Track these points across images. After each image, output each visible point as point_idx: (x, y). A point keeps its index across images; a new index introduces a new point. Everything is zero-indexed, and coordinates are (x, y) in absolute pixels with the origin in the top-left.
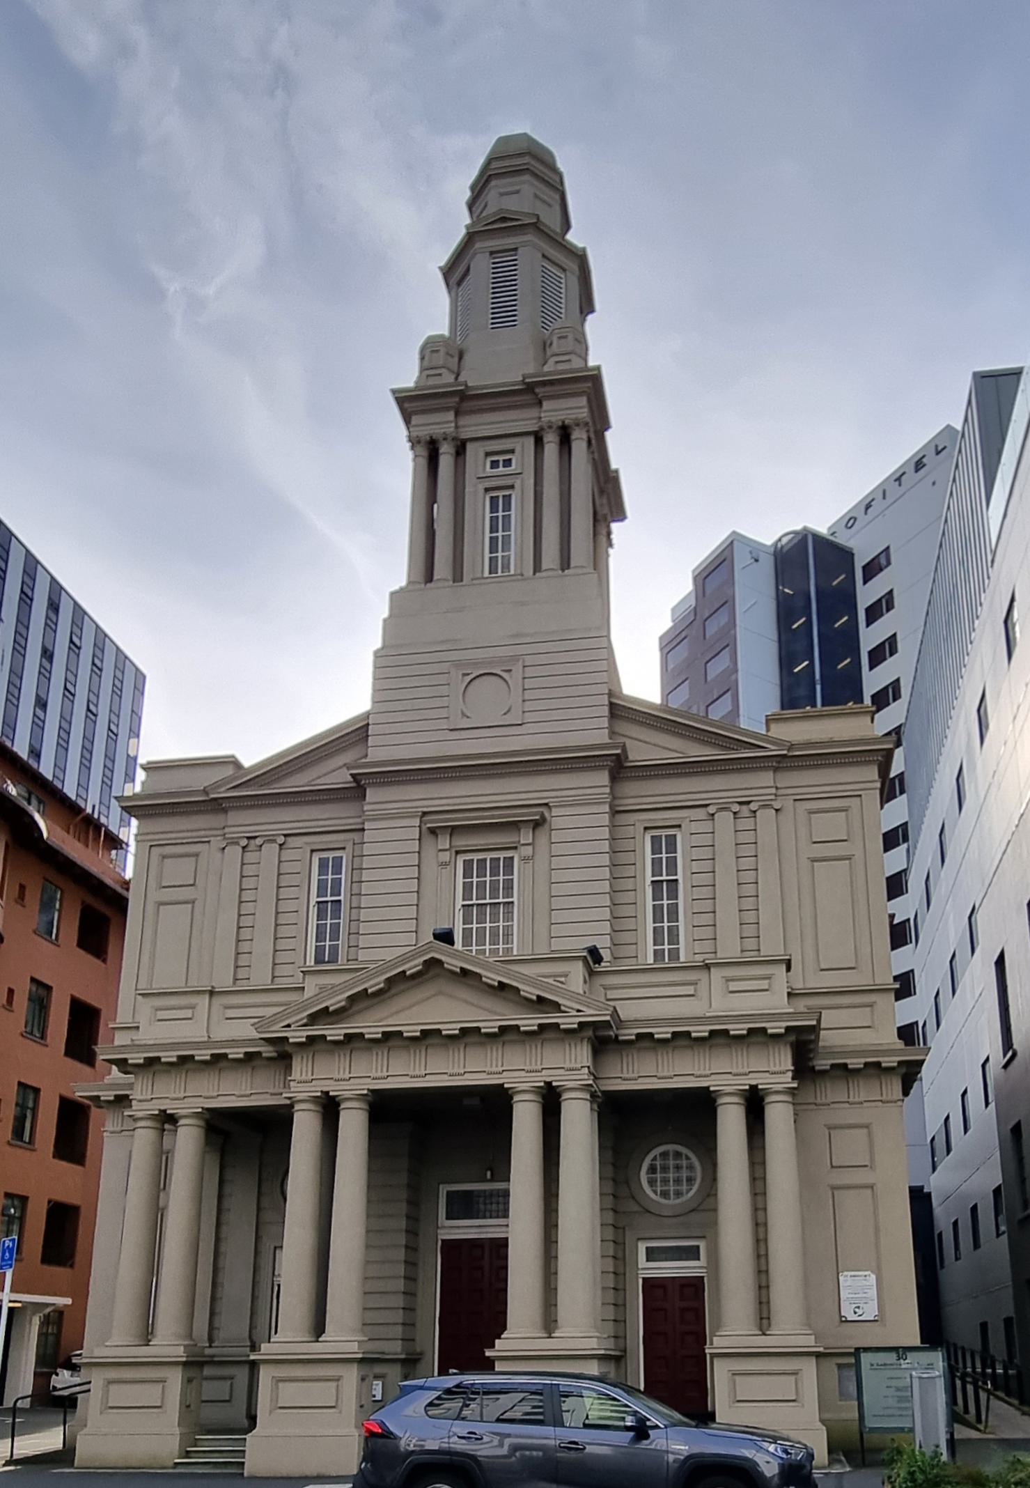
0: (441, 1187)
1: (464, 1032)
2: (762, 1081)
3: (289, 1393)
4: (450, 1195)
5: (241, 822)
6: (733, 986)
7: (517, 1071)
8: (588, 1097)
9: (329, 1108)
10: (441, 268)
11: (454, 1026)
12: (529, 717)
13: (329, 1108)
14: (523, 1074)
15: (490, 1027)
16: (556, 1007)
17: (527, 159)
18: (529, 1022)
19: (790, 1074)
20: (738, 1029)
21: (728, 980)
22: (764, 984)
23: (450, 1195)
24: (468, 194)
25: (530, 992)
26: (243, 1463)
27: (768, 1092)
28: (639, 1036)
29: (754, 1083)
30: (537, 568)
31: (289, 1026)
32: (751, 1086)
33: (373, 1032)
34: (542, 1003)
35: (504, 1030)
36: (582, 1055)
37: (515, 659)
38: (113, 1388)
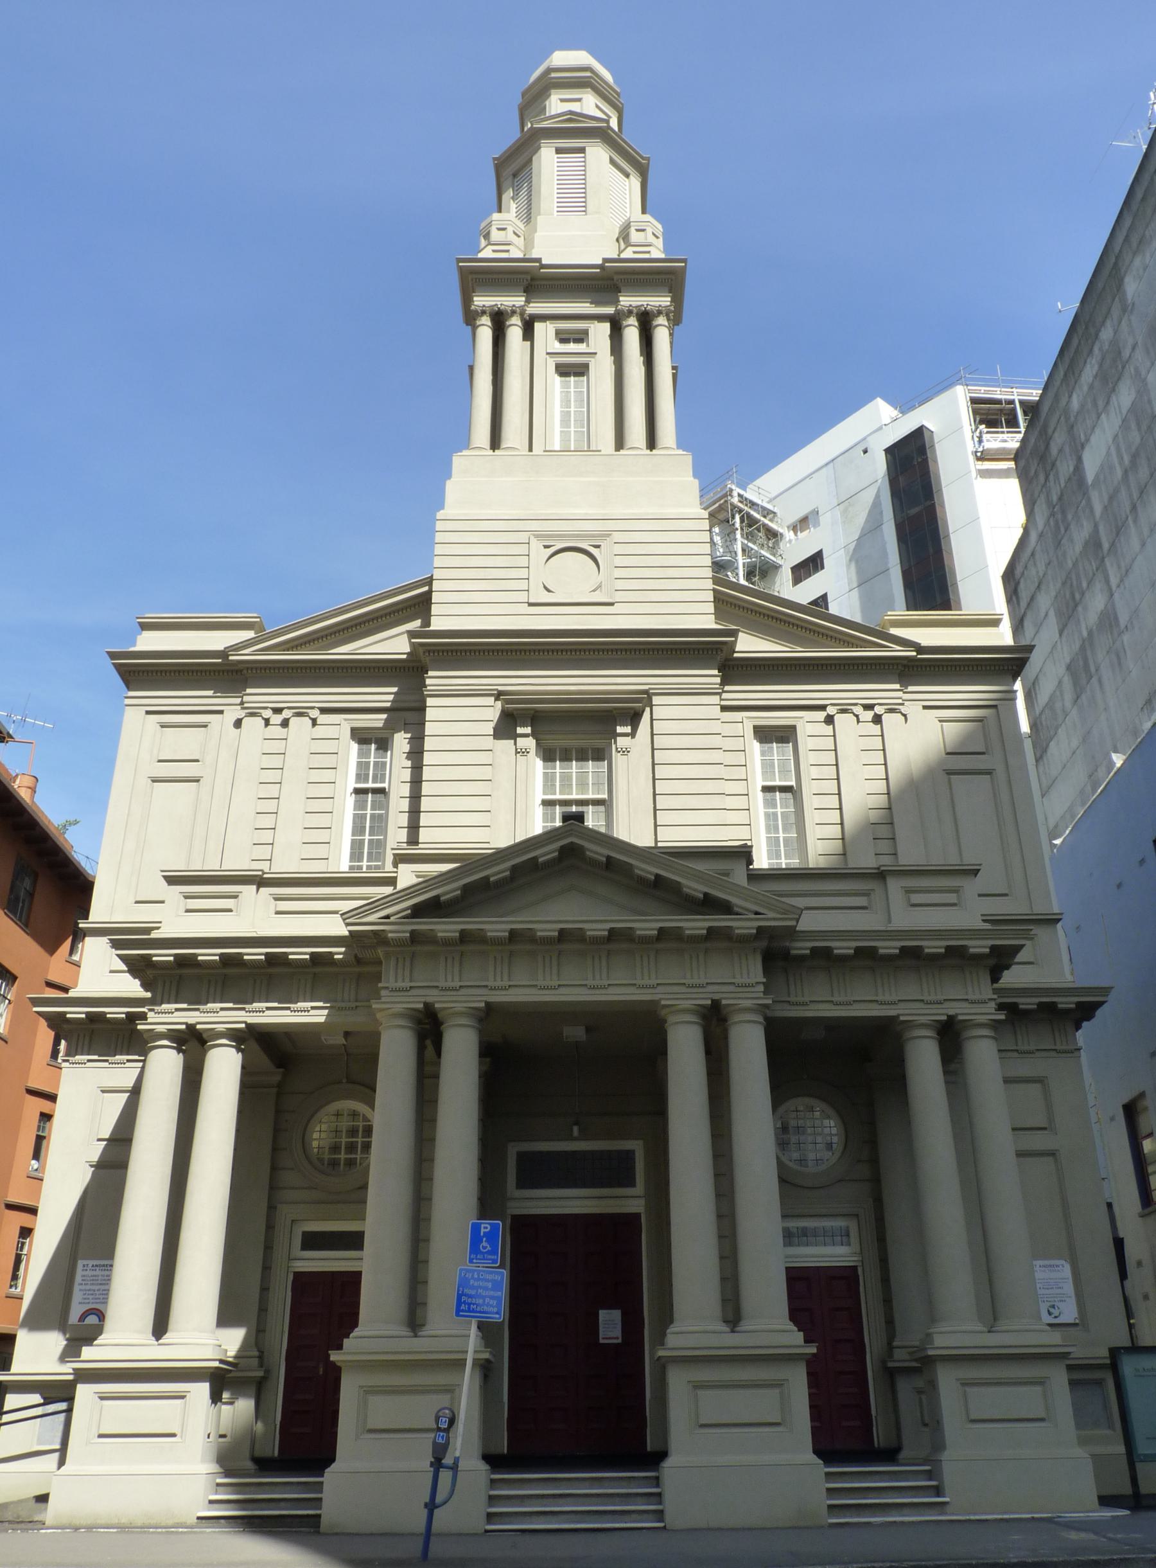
1: (563, 935)
2: (961, 1011)
3: (714, 1405)
4: (522, 1157)
5: (259, 696)
6: (917, 898)
7: (674, 990)
8: (761, 1019)
9: (429, 1029)
10: (494, 159)
11: (600, 926)
12: (618, 597)
13: (429, 1029)
14: (683, 989)
16: (725, 908)
17: (588, 74)
18: (647, 926)
19: (761, 988)
20: (934, 947)
21: (909, 891)
22: (951, 898)
23: (522, 1157)
24: (519, 100)
25: (695, 888)
27: (968, 1024)
28: (814, 950)
29: (951, 1012)
30: (620, 443)
31: (387, 917)
34: (710, 904)
35: (614, 935)
36: (753, 971)
37: (606, 535)
38: (374, 1400)
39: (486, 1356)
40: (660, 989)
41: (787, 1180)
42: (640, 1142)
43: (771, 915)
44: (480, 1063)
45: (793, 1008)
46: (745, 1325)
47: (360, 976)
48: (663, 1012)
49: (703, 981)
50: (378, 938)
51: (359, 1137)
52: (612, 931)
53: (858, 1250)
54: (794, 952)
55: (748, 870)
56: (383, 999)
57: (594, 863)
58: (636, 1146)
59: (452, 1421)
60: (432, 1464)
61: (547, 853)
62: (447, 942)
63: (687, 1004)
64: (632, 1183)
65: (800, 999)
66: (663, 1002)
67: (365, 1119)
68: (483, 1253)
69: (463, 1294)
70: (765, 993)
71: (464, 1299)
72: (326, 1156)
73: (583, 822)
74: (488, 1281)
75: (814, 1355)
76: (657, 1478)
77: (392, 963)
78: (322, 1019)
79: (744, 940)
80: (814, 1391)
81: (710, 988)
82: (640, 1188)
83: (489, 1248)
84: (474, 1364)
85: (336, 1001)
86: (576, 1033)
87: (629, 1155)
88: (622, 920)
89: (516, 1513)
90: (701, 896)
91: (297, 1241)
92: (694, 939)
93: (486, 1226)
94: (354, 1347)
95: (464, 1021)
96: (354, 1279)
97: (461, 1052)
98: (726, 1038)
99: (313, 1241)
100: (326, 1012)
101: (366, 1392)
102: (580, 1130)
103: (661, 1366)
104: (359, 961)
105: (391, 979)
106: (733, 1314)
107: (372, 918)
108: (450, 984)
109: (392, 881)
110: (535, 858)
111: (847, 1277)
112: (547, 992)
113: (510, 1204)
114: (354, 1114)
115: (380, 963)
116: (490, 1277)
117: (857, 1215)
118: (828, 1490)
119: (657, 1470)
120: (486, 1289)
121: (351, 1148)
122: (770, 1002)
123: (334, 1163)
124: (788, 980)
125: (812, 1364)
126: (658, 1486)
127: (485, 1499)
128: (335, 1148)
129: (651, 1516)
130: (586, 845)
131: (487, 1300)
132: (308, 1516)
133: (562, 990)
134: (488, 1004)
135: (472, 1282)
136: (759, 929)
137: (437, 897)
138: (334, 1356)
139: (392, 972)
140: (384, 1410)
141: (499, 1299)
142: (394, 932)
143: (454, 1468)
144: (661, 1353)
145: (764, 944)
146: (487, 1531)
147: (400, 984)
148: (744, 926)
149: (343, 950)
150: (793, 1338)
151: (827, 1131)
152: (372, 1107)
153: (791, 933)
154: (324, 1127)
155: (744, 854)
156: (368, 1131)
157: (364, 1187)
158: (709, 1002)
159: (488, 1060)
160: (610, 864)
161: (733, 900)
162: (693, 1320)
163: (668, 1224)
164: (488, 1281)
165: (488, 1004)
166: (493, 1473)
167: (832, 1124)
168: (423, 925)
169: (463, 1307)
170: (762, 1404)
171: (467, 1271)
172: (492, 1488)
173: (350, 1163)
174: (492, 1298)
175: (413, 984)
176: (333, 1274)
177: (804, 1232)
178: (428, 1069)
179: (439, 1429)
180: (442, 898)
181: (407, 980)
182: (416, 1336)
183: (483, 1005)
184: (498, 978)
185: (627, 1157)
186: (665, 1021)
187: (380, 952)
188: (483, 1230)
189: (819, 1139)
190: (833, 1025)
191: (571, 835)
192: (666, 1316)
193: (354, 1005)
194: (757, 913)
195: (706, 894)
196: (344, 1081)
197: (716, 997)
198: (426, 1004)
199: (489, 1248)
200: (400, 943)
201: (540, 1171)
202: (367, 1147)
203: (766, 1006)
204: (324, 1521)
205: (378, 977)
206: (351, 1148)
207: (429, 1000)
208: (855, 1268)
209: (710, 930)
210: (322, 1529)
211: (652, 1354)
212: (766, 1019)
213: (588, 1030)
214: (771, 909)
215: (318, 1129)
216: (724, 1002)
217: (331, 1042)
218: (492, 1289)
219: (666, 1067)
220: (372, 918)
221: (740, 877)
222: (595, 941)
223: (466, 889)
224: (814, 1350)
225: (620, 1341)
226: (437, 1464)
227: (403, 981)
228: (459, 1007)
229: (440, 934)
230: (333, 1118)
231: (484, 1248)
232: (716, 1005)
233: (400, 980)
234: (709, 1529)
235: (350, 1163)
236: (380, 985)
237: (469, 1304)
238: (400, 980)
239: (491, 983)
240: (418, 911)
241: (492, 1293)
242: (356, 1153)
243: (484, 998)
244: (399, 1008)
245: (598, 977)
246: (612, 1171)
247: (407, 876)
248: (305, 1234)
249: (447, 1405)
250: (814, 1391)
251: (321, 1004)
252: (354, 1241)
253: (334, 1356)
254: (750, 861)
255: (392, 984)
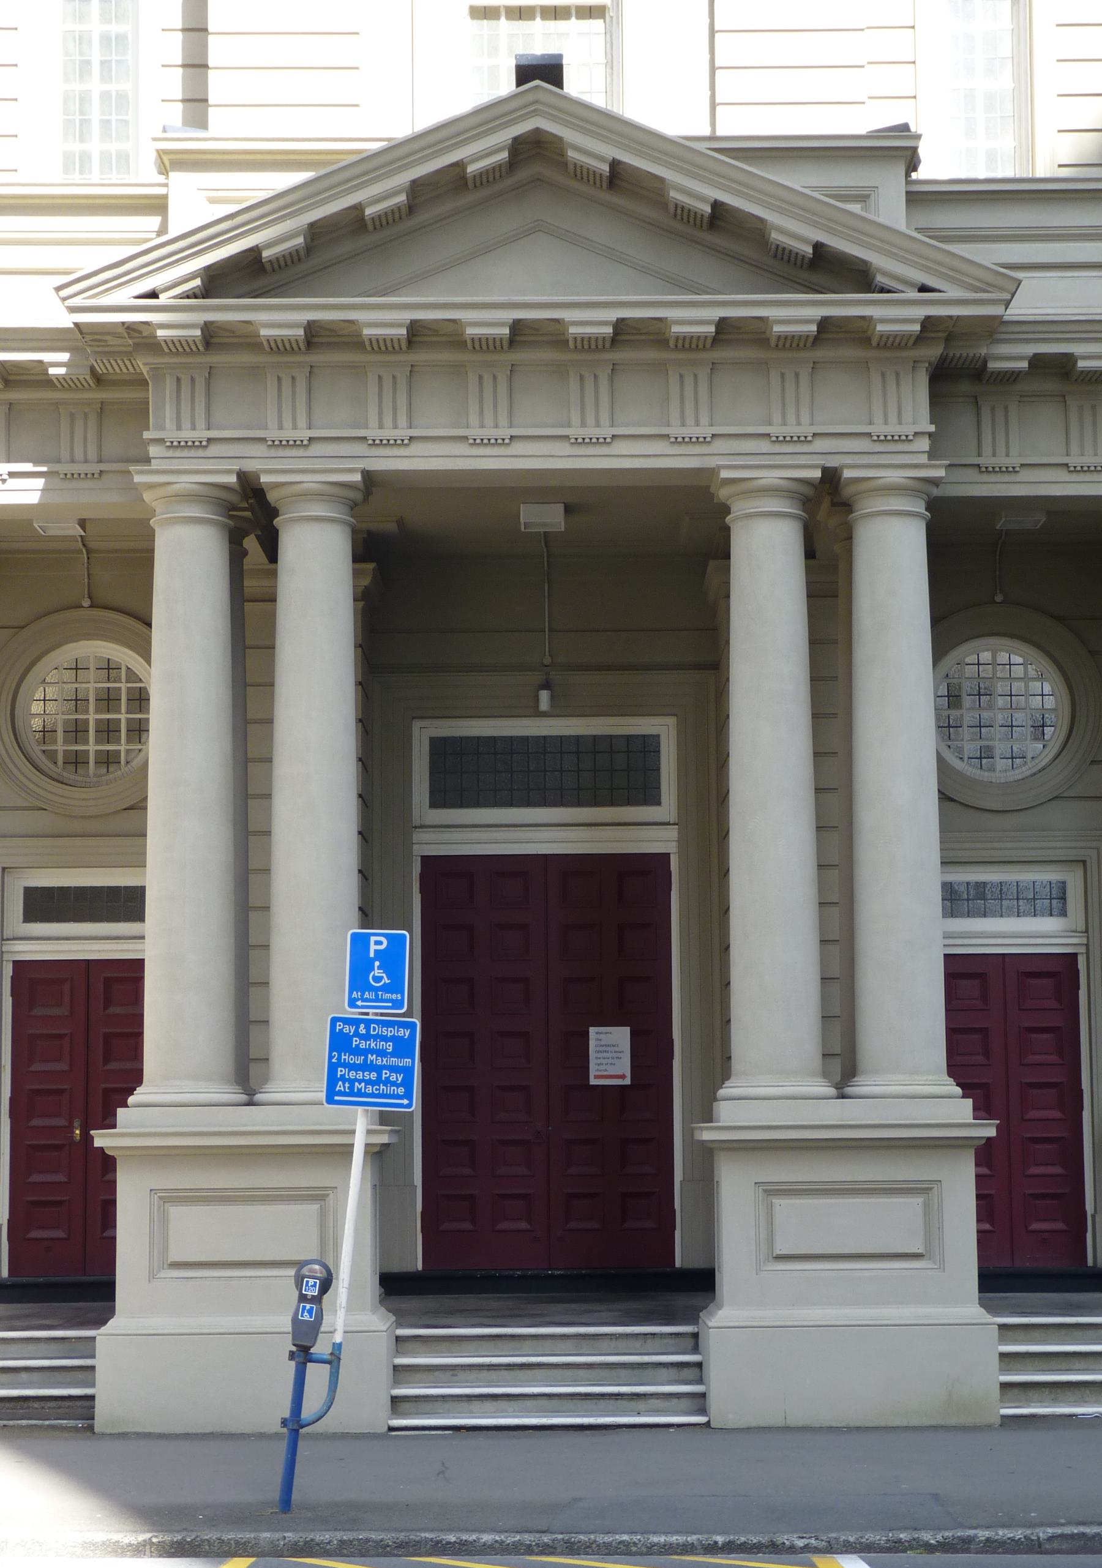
0: (417, 725)
1: (520, 333)
4: (440, 748)
7: (746, 446)
8: (920, 507)
9: (251, 521)
14: (764, 446)
15: (595, 322)
16: (858, 277)
18: (693, 315)
19: (924, 444)
23: (440, 748)
25: (797, 233)
26: (92, 1398)
28: (1037, 361)
31: (153, 295)
32: (825, 470)
33: (487, 322)
34: (826, 268)
35: (623, 333)
36: (910, 408)
39: (384, 1139)
40: (719, 446)
41: (958, 801)
42: (671, 721)
43: (953, 292)
44: (356, 574)
45: (986, 478)
46: (864, 1085)
47: (103, 409)
48: (723, 494)
49: (807, 430)
50: (139, 338)
51: (124, 710)
52: (620, 326)
53: (1081, 926)
54: (993, 365)
55: (909, 182)
56: (155, 465)
57: (582, 174)
58: (664, 730)
59: (326, 1284)
60: (292, 1356)
61: (484, 153)
62: (280, 348)
63: (771, 477)
64: (651, 797)
65: (1002, 460)
66: (724, 474)
67: (132, 676)
68: (372, 989)
69: (340, 1064)
70: (932, 454)
71: (341, 1071)
72: (60, 747)
73: (559, 84)
74: (385, 1039)
75: (989, 1139)
76: (695, 1336)
77: (169, 384)
78: (33, 498)
79: (893, 344)
80: (985, 1171)
81: (819, 445)
82: (668, 806)
83: (386, 980)
84: (366, 1153)
85: (59, 461)
86: (549, 518)
87: (648, 746)
88: (641, 303)
89: (444, 1397)
90: (809, 250)
91: (16, 905)
92: (791, 343)
93: (378, 941)
94: (132, 1127)
95: (319, 510)
96: (127, 977)
97: (317, 575)
98: (848, 538)
99: (45, 905)
100: (40, 483)
101: (164, 1200)
102: (553, 698)
103: (706, 1157)
104: (99, 380)
105: (168, 421)
106: (843, 1062)
107: (124, 296)
108: (289, 434)
109: (157, 206)
110: (460, 165)
111: (1057, 975)
112: (489, 451)
113: (418, 836)
114: (109, 668)
115: (143, 383)
116: (389, 1032)
117: (1084, 862)
118: (1002, 1355)
119: (694, 1319)
120: (382, 1053)
121: (108, 731)
122: (941, 473)
123: (77, 761)
124: (978, 414)
125: (985, 1153)
126: (696, 1350)
127: (386, 1374)
128: (77, 731)
129: (684, 1403)
130: (568, 135)
131: (385, 1074)
132: (70, 1398)
133: (518, 448)
134: (367, 475)
135: (355, 1041)
136: (928, 323)
137: (255, 251)
138: (101, 1139)
139: (169, 412)
140: (197, 1231)
141: (408, 1072)
142: (170, 323)
143: (334, 1360)
144: (707, 1136)
145: (934, 352)
146: (391, 1429)
147: (187, 434)
148: (894, 315)
149: (65, 357)
150: (955, 1112)
151: (1036, 702)
152: (147, 656)
153: (992, 329)
154: (51, 692)
155: (897, 149)
156: (140, 699)
157: (140, 806)
158: (817, 474)
159: (371, 566)
160: (617, 177)
161: (876, 259)
162: (766, 1076)
163: (725, 873)
164: (385, 1039)
165: (367, 475)
166: (400, 1325)
167: (1047, 688)
168: (228, 312)
169: (340, 1087)
170: (894, 1221)
171: (347, 1021)
172: (398, 1353)
173: (108, 760)
174: (394, 1069)
175: (213, 434)
176: (88, 965)
177: (980, 890)
178: (250, 584)
179: (303, 1298)
180: (265, 254)
181: (201, 423)
182: (250, 1103)
183: (357, 477)
184: (388, 421)
185: (646, 749)
186: (726, 510)
187: (143, 364)
188: (373, 948)
189: (1019, 717)
190: (1059, 510)
191: (534, 113)
192: (718, 1063)
193: (96, 468)
194: (923, 289)
195: (818, 247)
196: (86, 603)
197: (832, 462)
198: (242, 476)
199: (386, 980)
200: (178, 347)
201: (471, 774)
202: (139, 730)
203: (935, 482)
204: (101, 1408)
205: (140, 414)
206: (108, 731)
207: (250, 466)
208: (1074, 956)
209: (824, 324)
210: (99, 1424)
211: (688, 1133)
212: (935, 505)
213: (569, 510)
214: (953, 281)
215: (39, 695)
216: (847, 474)
217: (51, 532)
218: (393, 1055)
219: (727, 583)
220: (124, 296)
221: (891, 209)
222: (590, 345)
223: (317, 233)
224: (992, 1132)
225: (627, 1081)
226: (303, 1354)
227: (194, 428)
228: (310, 482)
229: (264, 332)
230: (69, 675)
231: (377, 979)
232: (831, 478)
233: (186, 424)
234: (787, 1429)
235: (108, 760)
236: (147, 435)
237: (352, 1082)
238: (186, 424)
239: (371, 433)
240: (217, 282)
241: (394, 1061)
242: (118, 741)
243: (361, 465)
244: (186, 482)
245: (590, 420)
246: (617, 774)
247: (195, 202)
248: (29, 892)
249: (315, 1256)
250: (985, 1171)
251: (28, 467)
252: (127, 904)
253: (101, 1139)
254: (913, 164)
255: (170, 433)
